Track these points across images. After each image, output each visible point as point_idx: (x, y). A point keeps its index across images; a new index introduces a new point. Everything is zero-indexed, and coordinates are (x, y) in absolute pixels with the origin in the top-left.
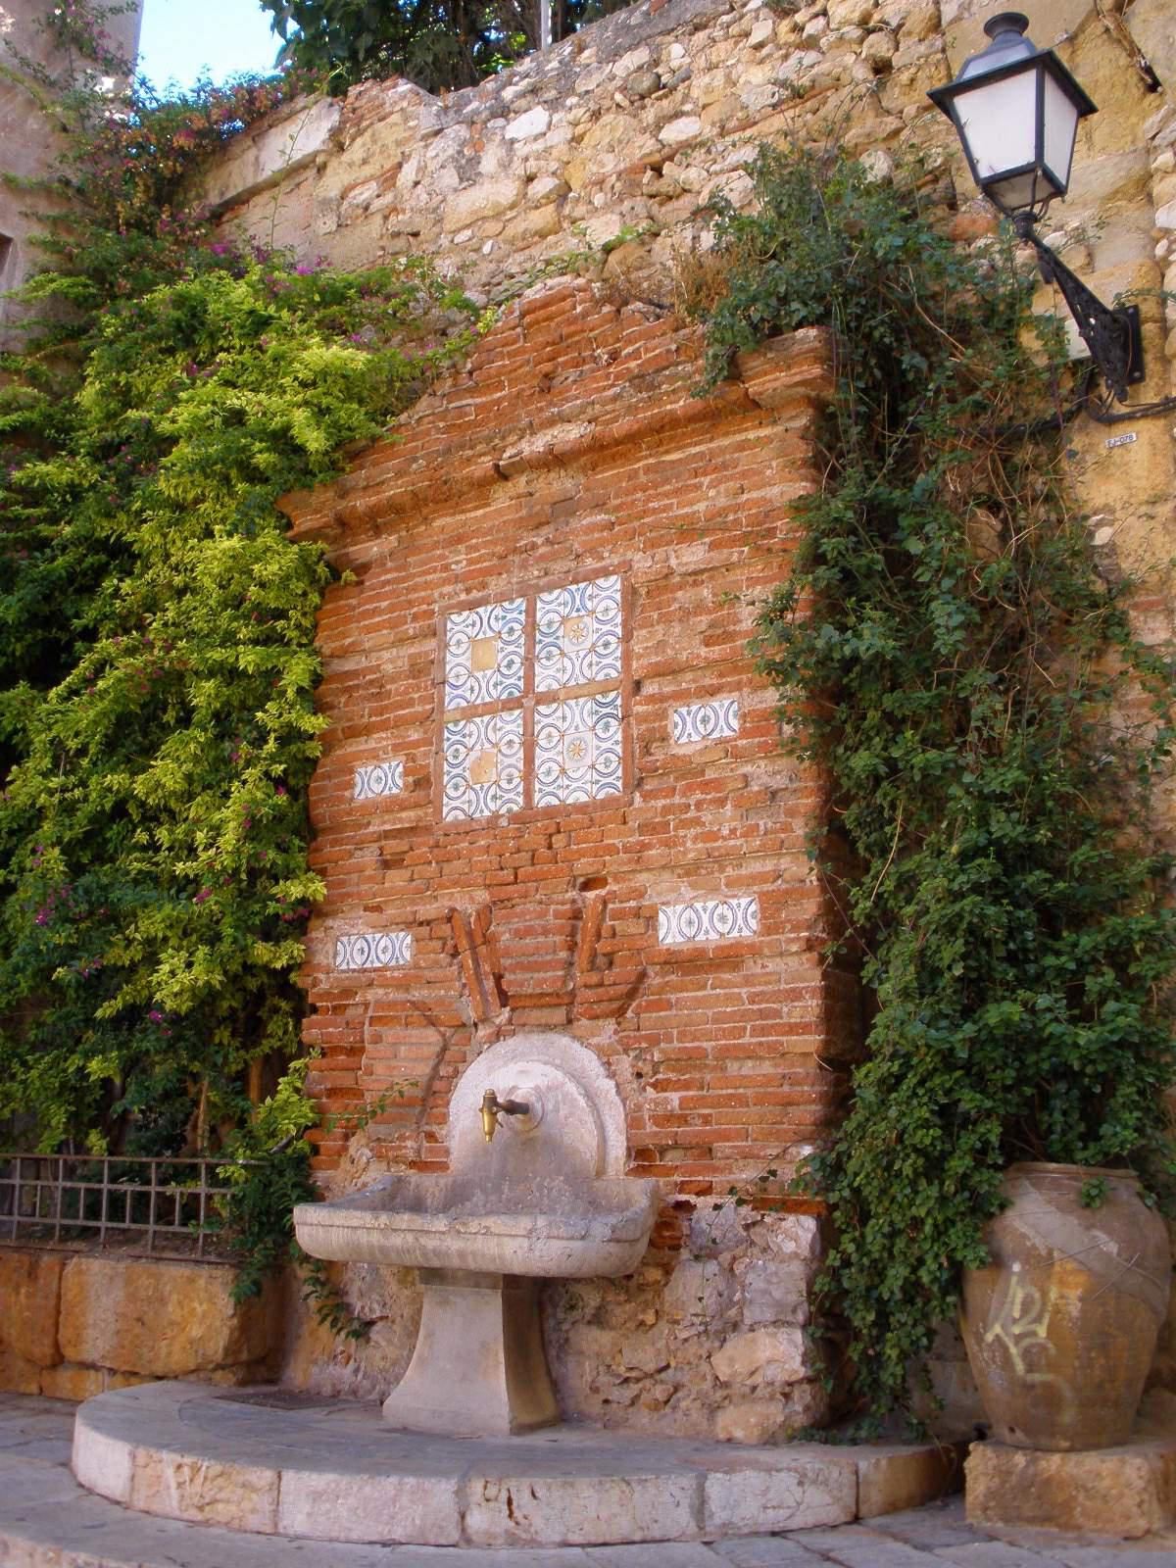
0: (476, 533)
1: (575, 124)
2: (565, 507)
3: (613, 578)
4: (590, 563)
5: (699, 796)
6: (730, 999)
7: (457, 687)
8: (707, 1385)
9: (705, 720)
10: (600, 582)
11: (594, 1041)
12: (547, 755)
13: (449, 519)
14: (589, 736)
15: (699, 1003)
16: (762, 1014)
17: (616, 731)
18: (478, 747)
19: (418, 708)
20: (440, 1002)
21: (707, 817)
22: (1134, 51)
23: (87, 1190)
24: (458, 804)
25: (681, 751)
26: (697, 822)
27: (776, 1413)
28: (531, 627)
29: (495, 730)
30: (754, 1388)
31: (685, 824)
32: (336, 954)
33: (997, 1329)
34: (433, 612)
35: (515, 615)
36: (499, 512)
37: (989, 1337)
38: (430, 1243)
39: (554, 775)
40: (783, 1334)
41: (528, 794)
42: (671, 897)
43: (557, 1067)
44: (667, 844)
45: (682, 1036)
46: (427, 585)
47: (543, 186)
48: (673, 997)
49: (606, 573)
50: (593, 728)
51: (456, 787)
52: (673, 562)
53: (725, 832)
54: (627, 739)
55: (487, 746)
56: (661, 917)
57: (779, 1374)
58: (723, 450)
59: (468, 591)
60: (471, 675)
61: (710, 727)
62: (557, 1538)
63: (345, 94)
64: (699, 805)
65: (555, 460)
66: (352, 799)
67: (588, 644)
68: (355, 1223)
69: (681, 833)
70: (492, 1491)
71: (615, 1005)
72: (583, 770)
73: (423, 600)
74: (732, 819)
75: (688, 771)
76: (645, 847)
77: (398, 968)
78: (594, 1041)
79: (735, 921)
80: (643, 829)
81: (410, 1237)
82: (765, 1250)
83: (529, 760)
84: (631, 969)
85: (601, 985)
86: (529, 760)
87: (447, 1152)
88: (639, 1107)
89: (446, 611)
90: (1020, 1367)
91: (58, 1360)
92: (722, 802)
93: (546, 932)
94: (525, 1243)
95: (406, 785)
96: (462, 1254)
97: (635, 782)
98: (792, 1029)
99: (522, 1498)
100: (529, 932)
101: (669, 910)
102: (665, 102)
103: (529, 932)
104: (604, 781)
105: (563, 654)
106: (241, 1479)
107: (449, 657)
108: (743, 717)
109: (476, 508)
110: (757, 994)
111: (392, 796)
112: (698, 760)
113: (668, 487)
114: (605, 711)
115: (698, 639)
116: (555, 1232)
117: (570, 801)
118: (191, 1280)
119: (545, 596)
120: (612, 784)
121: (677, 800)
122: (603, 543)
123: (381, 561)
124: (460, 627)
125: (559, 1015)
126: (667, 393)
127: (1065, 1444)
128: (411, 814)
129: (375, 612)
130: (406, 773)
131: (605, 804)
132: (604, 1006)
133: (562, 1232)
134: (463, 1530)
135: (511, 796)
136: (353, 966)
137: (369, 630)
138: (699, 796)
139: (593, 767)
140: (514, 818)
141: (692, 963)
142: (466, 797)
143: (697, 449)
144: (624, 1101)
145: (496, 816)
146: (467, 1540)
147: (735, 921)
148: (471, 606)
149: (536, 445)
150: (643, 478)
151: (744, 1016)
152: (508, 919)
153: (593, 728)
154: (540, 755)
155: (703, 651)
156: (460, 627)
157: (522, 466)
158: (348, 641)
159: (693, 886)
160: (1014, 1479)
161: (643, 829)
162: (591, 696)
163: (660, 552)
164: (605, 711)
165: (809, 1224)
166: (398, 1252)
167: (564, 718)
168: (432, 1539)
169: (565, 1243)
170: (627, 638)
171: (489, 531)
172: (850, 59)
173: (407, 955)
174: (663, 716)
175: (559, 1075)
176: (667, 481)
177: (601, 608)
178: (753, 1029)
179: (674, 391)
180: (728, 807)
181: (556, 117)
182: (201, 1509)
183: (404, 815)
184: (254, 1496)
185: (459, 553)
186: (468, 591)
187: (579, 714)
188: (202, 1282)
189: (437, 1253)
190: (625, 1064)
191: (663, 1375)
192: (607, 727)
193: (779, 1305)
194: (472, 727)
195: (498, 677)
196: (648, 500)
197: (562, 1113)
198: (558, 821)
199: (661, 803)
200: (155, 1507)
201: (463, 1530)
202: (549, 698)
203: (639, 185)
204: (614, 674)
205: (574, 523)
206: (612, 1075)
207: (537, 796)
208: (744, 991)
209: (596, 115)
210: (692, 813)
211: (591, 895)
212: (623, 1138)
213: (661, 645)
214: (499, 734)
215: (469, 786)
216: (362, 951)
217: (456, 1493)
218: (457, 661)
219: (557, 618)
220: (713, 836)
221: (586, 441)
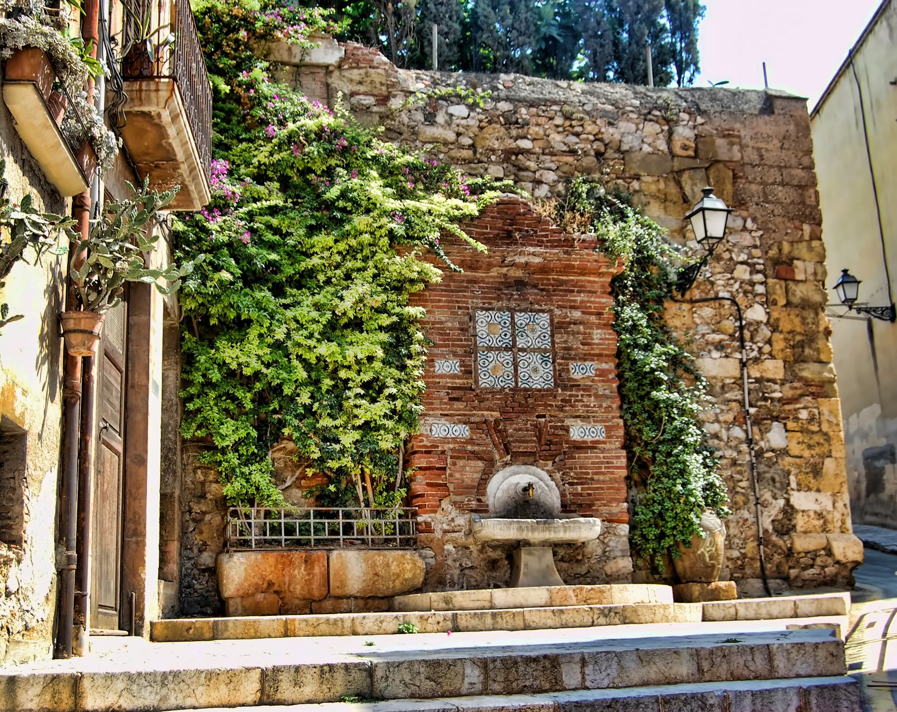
1: (481, 121)
4: (537, 307)
6: (597, 457)
8: (604, 576)
14: (540, 366)
15: (587, 458)
16: (608, 463)
20: (484, 452)
21: (585, 400)
22: (681, 188)
24: (485, 382)
26: (581, 401)
28: (513, 323)
33: (702, 550)
36: (491, 277)
37: (699, 552)
40: (625, 559)
44: (572, 406)
45: (581, 468)
47: (466, 141)
49: (543, 311)
52: (569, 314)
58: (582, 281)
59: (484, 303)
64: (582, 395)
67: (537, 335)
73: (464, 302)
76: (564, 406)
82: (615, 534)
83: (516, 370)
86: (516, 370)
87: (487, 506)
88: (564, 490)
90: (708, 559)
93: (527, 430)
95: (461, 371)
98: (618, 468)
100: (520, 430)
102: (520, 130)
103: (520, 430)
118: (403, 556)
122: (542, 301)
125: (531, 459)
130: (461, 366)
131: (548, 390)
140: (511, 390)
141: (580, 447)
145: (503, 388)
148: (487, 310)
150: (552, 282)
151: (602, 463)
152: (511, 424)
161: (562, 400)
163: (564, 310)
165: (627, 526)
170: (552, 336)
171: (488, 283)
172: (589, 146)
173: (467, 433)
177: (542, 323)
181: (472, 114)
186: (484, 303)
187: (536, 359)
188: (408, 556)
190: (558, 476)
192: (546, 364)
193: (622, 551)
195: (500, 338)
198: (528, 393)
203: (510, 159)
206: (553, 480)
207: (520, 384)
208: (601, 455)
209: (490, 122)
210: (580, 398)
220: (589, 406)
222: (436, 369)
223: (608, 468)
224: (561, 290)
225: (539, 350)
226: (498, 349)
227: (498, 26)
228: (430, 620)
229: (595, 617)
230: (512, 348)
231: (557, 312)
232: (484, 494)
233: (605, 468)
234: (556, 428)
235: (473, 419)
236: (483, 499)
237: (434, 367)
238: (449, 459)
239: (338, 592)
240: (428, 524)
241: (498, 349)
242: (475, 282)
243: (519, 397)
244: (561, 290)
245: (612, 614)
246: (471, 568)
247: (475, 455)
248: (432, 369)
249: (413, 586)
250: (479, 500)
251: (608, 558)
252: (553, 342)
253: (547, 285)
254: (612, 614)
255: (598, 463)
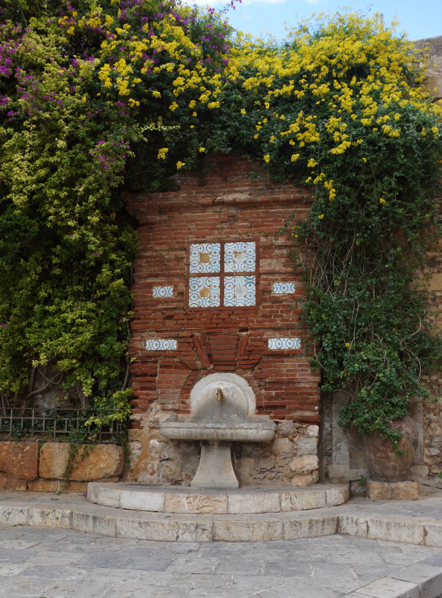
0: (199, 221)
2: (233, 218)
3: (253, 243)
5: (282, 309)
7: (194, 267)
9: (284, 288)
10: (248, 243)
11: (245, 375)
12: (229, 291)
13: (189, 214)
17: (253, 287)
18: (203, 286)
19: (178, 271)
21: (284, 315)
23: (24, 419)
25: (276, 295)
27: (309, 478)
29: (209, 281)
30: (303, 472)
31: (278, 316)
32: (145, 345)
34: (184, 242)
35: (216, 248)
38: (220, 431)
39: (231, 298)
40: (311, 457)
41: (222, 301)
42: (273, 336)
43: (232, 382)
46: (182, 233)
48: (273, 364)
50: (245, 285)
51: (194, 297)
53: (291, 320)
54: (257, 290)
55: (206, 286)
56: (269, 342)
57: (309, 468)
60: (199, 263)
61: (285, 290)
62: (301, 508)
63: (261, 84)
65: (234, 204)
66: (152, 296)
68: (191, 426)
69: (276, 319)
70: (287, 497)
71: (252, 366)
72: (241, 297)
74: (293, 316)
75: (277, 300)
76: (263, 321)
77: (172, 351)
78: (245, 375)
79: (294, 344)
80: (263, 316)
81: (212, 430)
84: (258, 356)
85: (248, 360)
89: (190, 243)
91: (38, 477)
92: (289, 311)
94: (255, 431)
96: (232, 435)
97: (259, 301)
99: (294, 498)
101: (272, 340)
104: (249, 301)
105: (234, 262)
106: (214, 499)
107: (191, 257)
108: (296, 288)
109: (200, 212)
110: (300, 365)
111: (168, 297)
112: (281, 298)
113: (270, 219)
114: (249, 281)
115: (282, 265)
116: (264, 428)
117: (237, 306)
119: (228, 244)
120: (251, 302)
121: (274, 309)
123: (160, 222)
124: (195, 249)
126: (277, 192)
127: (395, 480)
128: (175, 304)
129: (161, 239)
130: (174, 291)
132: (248, 366)
133: (266, 428)
134: (281, 507)
135: (215, 302)
136: (153, 349)
137: (157, 244)
138: (282, 309)
139: (245, 296)
142: (198, 301)
143: (280, 210)
144: (255, 393)
146: (282, 510)
147: (294, 344)
148: (200, 242)
149: (230, 198)
150: (262, 215)
153: (245, 285)
154: (226, 291)
155: (284, 269)
156: (195, 249)
157: (223, 203)
158: (149, 246)
159: (280, 334)
160: (385, 489)
161: (263, 316)
162: (245, 276)
164: (249, 281)
166: (207, 435)
167: (235, 281)
168: (273, 511)
169: (266, 431)
174: (270, 285)
175: (234, 385)
176: (269, 218)
177: (249, 250)
178: (299, 374)
179: (279, 192)
180: (292, 313)
182: (198, 509)
183: (173, 303)
184: (220, 503)
185: (192, 225)
189: (222, 435)
191: (273, 470)
192: (250, 286)
194: (201, 280)
196: (264, 222)
197: (235, 396)
199: (269, 309)
200: (178, 510)
201: (281, 507)
202: (214, 275)
204: (253, 271)
205: (237, 224)
211: (244, 333)
212: (255, 404)
213: (270, 264)
214: (211, 283)
215: (199, 297)
216: (157, 345)
217: (279, 497)
218: (194, 259)
219: (232, 251)
221: (247, 200)
222: (154, 294)
223: (302, 375)
224: (269, 221)
225: (246, 274)
226: (210, 275)
227: (387, 266)
228: (50, 516)
229: (180, 532)
230: (222, 274)
231: (263, 240)
232: (188, 397)
233: (300, 375)
234: (255, 340)
235: (181, 334)
236: (187, 401)
237: (152, 293)
238: (158, 368)
239: (47, 476)
240: (139, 422)
241: (210, 275)
242: (193, 221)
243: (223, 315)
244: (269, 221)
245: (200, 531)
246: (168, 459)
247: (184, 366)
248: (150, 295)
249: (107, 474)
250: (183, 402)
251: (295, 455)
252: (258, 266)
253: (256, 218)
254: (200, 531)
255: (292, 370)
